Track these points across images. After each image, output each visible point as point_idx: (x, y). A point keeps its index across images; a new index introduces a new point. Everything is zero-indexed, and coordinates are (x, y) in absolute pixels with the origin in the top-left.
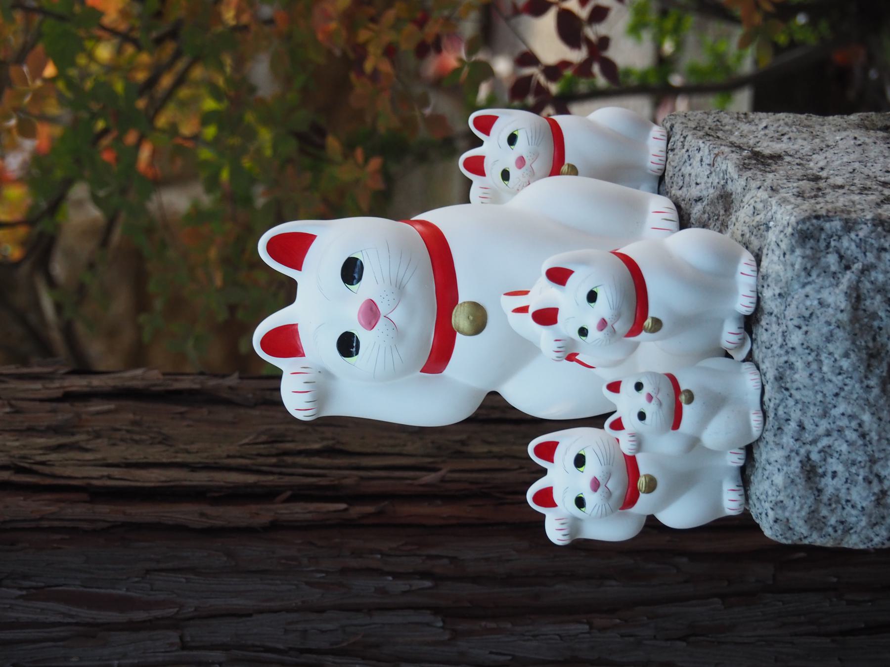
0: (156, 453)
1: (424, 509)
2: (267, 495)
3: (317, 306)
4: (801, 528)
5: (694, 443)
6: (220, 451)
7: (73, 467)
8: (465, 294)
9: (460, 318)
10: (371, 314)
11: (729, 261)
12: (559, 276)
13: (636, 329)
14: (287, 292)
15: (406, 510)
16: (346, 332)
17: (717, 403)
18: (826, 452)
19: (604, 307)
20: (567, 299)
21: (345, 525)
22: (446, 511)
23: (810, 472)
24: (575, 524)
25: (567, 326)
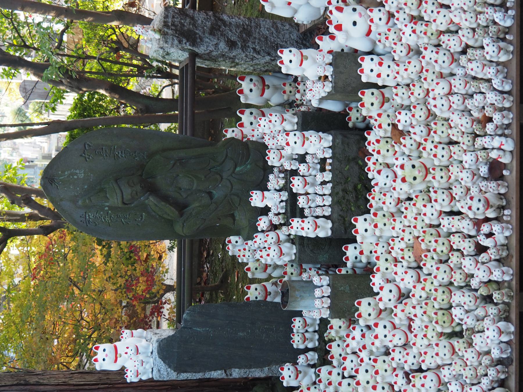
0: (83, 380)
1: (119, 385)
2: (98, 384)
3: (100, 355)
4: (158, 378)
5: (145, 368)
6: (92, 379)
7: (71, 382)
8: (119, 352)
9: (118, 356)
10: (107, 355)
11: (149, 345)
12: (128, 348)
13: (137, 354)
14: (96, 354)
15: (116, 386)
16: (104, 359)
17: (147, 363)
18: (161, 368)
19: (133, 351)
20: (128, 351)
21: (108, 388)
22: (122, 385)
23: (159, 371)
24: (131, 380)
25: (129, 354)
